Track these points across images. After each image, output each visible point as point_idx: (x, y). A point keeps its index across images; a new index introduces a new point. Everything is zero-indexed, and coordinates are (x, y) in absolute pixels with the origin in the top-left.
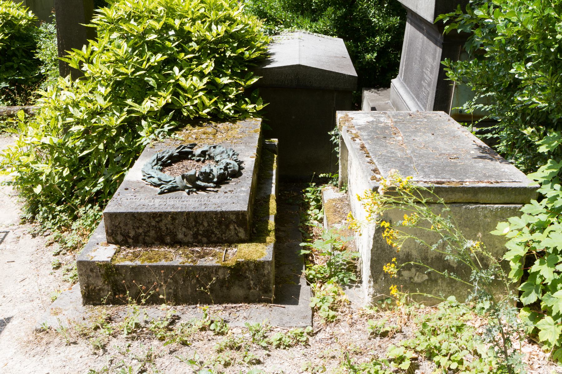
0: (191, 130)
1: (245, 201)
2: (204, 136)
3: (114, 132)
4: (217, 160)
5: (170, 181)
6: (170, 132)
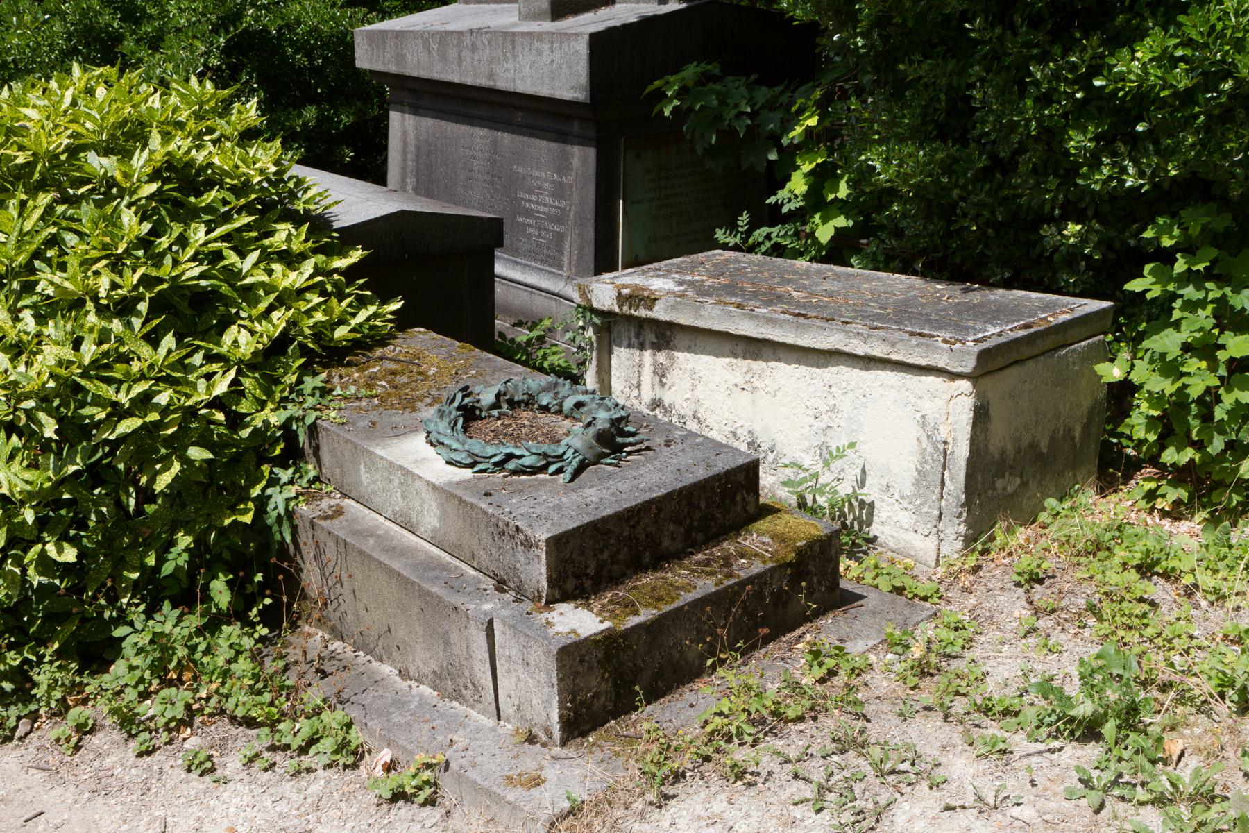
5: (564, 453)
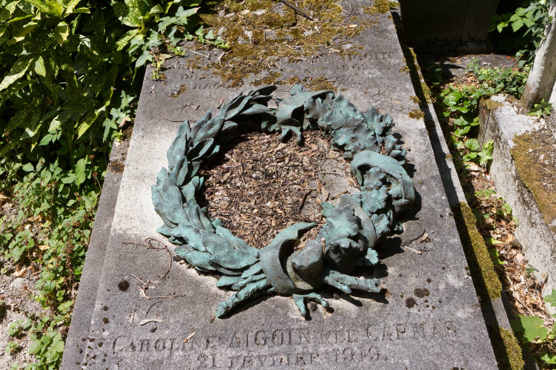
0: (236, 11)
1: (481, 350)
2: (271, 33)
3: (63, 30)
4: (341, 142)
5: (247, 268)
6: (193, 24)
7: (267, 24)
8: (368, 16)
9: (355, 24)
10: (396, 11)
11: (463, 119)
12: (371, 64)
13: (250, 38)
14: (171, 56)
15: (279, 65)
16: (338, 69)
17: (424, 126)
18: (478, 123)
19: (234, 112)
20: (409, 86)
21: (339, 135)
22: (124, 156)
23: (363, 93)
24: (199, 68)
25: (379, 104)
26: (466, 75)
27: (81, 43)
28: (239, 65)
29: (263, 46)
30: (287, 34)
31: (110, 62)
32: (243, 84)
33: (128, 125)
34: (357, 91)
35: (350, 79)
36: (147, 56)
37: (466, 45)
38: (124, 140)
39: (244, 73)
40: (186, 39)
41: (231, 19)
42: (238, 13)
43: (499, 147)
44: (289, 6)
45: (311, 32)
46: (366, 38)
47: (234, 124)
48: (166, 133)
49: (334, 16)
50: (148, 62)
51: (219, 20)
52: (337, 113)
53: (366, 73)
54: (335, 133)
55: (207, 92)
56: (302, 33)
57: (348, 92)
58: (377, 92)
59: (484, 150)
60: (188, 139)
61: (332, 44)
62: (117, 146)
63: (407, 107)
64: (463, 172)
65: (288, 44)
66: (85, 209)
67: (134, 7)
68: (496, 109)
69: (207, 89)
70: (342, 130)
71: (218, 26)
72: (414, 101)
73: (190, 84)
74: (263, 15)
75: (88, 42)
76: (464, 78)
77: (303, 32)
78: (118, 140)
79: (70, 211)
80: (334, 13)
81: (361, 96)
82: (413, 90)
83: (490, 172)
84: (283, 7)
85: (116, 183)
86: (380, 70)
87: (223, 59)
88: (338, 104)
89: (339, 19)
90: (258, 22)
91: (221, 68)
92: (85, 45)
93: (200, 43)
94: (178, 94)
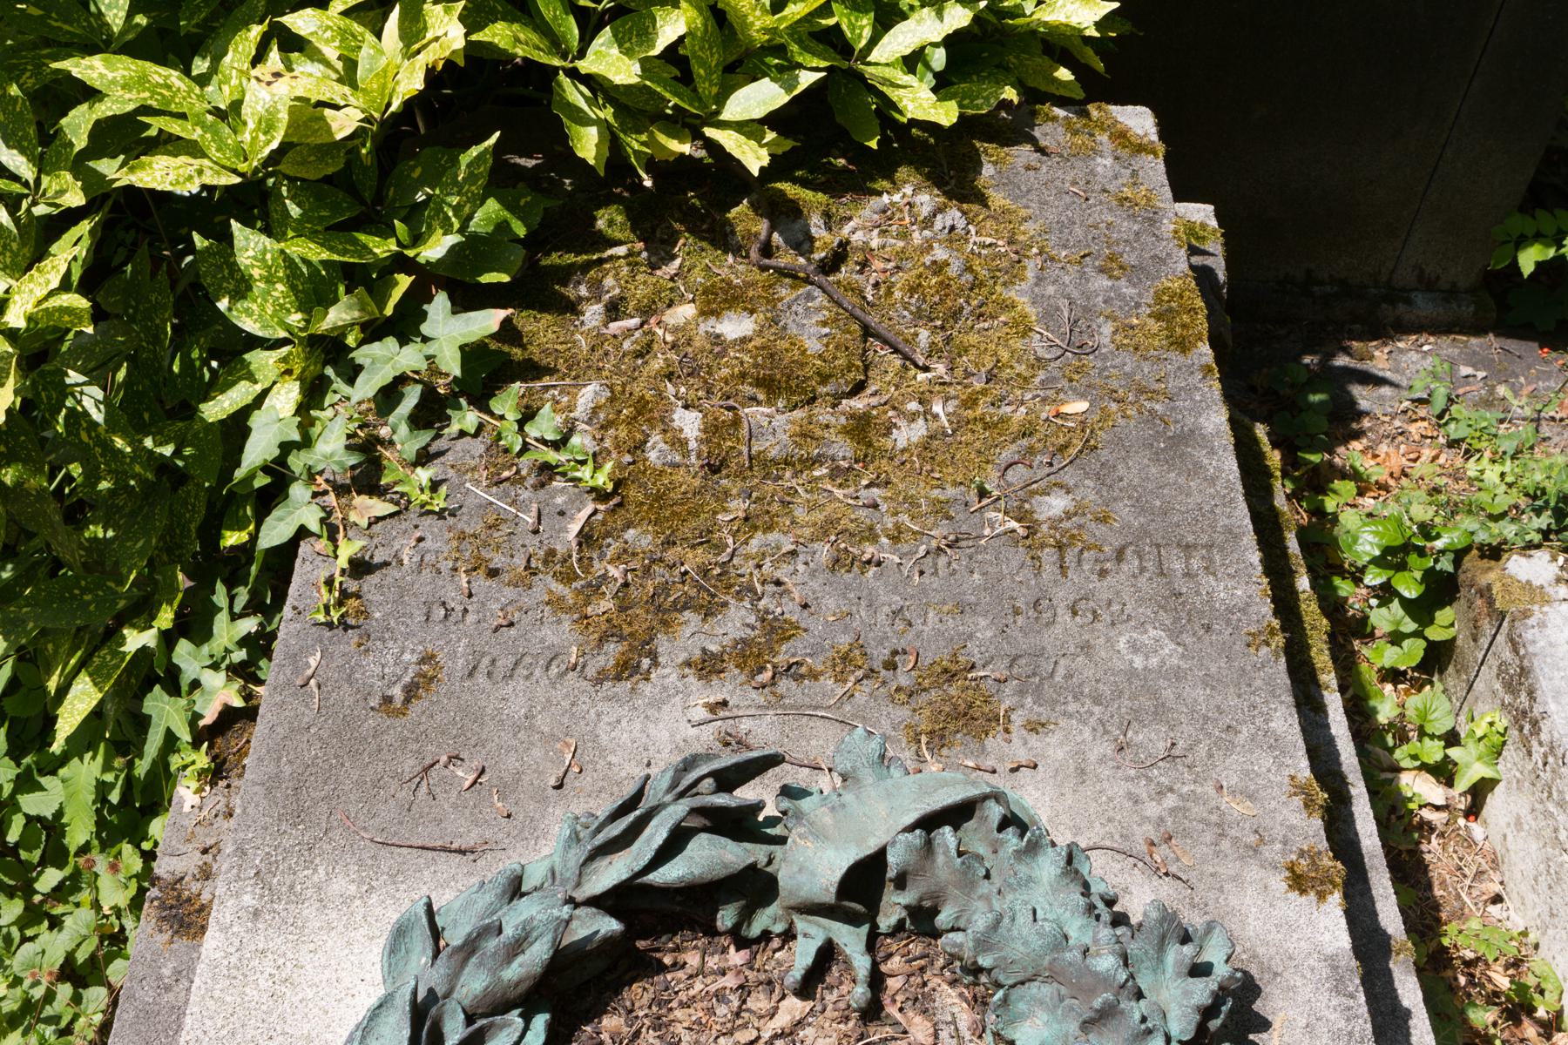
2: (771, 425)
6: (487, 371)
7: (759, 383)
8: (1129, 362)
9: (1083, 396)
10: (1209, 261)
11: (1401, 612)
12: (1141, 601)
13: (693, 445)
14: (392, 509)
15: (795, 576)
16: (1017, 612)
17: (1344, 941)
18: (1451, 632)
19: (612, 872)
20: (1285, 722)
21: (1022, 1006)
22: (208, 858)
23: (1107, 748)
24: (493, 573)
25: (1173, 811)
26: (1405, 412)
27: (69, 403)
28: (647, 571)
29: (739, 484)
30: (831, 435)
31: (180, 463)
32: (655, 663)
33: (229, 718)
34: (1087, 734)
35: (1061, 671)
36: (300, 510)
37: (1409, 302)
38: (213, 784)
39: (665, 612)
40: (455, 428)
41: (627, 345)
42: (653, 321)
43: (1530, 754)
44: (840, 305)
45: (919, 430)
46: (1121, 470)
47: (610, 925)
48: (347, 900)
49: (1005, 355)
50: (303, 533)
51: (584, 344)
52: (1020, 920)
53: (1122, 644)
54: (1005, 1000)
55: (515, 698)
56: (888, 433)
57: (1053, 739)
58: (1162, 746)
59: (1471, 745)
60: (421, 996)
61: (996, 493)
62: (187, 808)
63: (1279, 832)
64: (1396, 818)
65: (832, 477)
66: (96, 906)
67: (269, 280)
68: (1526, 614)
69: (519, 684)
70: (1033, 989)
71: (579, 371)
72: (1306, 806)
73: (455, 653)
74: (744, 340)
75: (97, 402)
76: (1397, 423)
77: (889, 428)
78: (194, 785)
79: (46, 907)
80: (1003, 341)
81: (1102, 760)
82: (1301, 744)
83: (1485, 812)
84: (819, 309)
85: (168, 989)
86: (1175, 635)
87: (586, 538)
88: (1023, 870)
89: (1021, 368)
90: (725, 372)
91: (577, 577)
92: (86, 414)
93: (506, 451)
94: (407, 701)
